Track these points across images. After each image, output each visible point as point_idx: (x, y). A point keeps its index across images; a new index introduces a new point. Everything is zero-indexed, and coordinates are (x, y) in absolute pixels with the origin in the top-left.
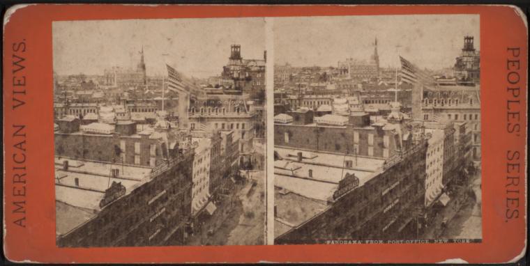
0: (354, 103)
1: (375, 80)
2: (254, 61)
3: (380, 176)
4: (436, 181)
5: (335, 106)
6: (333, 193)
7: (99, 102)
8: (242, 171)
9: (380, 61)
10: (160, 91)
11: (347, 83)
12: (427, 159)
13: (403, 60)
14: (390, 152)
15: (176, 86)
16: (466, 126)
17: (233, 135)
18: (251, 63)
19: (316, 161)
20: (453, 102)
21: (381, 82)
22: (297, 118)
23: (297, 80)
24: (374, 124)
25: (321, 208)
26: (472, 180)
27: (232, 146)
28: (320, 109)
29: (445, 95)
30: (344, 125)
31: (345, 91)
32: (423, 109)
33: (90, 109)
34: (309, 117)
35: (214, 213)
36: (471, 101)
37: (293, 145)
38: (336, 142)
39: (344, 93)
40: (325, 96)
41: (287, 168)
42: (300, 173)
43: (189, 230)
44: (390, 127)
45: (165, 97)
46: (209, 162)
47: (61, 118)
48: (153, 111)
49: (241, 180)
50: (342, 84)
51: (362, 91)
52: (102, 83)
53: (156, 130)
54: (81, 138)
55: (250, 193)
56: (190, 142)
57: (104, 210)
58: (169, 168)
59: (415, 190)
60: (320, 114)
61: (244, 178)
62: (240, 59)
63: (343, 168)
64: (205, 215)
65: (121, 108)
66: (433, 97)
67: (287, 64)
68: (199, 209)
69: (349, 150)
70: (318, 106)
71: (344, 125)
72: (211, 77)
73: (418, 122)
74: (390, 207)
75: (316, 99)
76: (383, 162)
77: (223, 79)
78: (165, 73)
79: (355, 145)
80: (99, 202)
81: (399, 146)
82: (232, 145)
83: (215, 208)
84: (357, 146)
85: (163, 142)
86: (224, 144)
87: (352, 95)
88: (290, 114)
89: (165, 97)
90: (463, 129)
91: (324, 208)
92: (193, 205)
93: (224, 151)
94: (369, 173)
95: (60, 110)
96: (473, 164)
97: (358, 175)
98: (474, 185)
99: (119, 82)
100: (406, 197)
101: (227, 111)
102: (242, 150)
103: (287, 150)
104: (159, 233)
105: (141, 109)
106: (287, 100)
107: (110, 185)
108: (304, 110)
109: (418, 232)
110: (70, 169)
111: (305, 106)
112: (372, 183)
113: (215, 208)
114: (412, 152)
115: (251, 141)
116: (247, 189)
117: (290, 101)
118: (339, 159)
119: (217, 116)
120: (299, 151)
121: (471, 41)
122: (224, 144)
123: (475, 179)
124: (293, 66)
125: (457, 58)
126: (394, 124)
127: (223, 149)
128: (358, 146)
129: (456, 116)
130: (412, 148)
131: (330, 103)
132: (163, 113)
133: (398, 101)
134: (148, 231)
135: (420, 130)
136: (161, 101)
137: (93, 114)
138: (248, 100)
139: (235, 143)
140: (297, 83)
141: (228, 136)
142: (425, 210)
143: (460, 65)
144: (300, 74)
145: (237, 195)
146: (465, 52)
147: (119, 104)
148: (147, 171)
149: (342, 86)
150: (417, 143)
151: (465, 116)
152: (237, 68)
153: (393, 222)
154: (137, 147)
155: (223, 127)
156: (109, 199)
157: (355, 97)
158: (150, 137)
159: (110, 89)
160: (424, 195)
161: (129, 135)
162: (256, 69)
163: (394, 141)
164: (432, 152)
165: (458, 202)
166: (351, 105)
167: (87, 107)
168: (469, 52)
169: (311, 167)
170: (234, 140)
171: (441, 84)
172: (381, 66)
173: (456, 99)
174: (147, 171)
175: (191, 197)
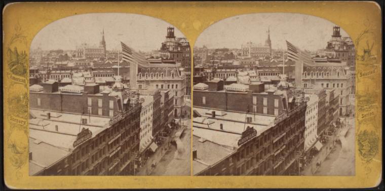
0: (253, 75)
1: (102, 59)
2: (184, 39)
3: (107, 130)
4: (312, 132)
5: (239, 77)
6: (73, 143)
7: (72, 70)
8: (176, 120)
9: (106, 47)
10: (116, 61)
11: (83, 62)
12: (306, 116)
13: (289, 44)
14: (114, 113)
15: (293, 56)
16: (334, 92)
17: (169, 93)
18: (182, 41)
19: (225, 117)
20: (160, 76)
21: (273, 60)
22: (211, 84)
23: (46, 60)
24: (267, 91)
25: (229, 152)
26: (339, 131)
27: (169, 102)
28: (63, 81)
29: (320, 69)
30: (81, 93)
31: (81, 68)
32: (138, 81)
33: (231, 73)
34: (220, 85)
35: (321, 149)
36: (338, 74)
37: (207, 105)
38: (241, 103)
39: (80, 69)
40: (67, 72)
41: (39, 124)
42: (212, 126)
43: (138, 163)
44: (279, 92)
45: (120, 65)
46: (152, 113)
47: (210, 80)
48: (111, 76)
49: (175, 126)
50: (79, 62)
51: (93, 68)
52: (240, 54)
53: (278, 88)
54: (224, 95)
55: (182, 136)
56: (138, 99)
57: (241, 148)
58: (124, 118)
59: (298, 138)
60: (64, 84)
61: (178, 125)
62: (174, 37)
63: (245, 123)
64: (151, 152)
65: (88, 74)
66: (145, 72)
67: (39, 48)
68: (310, 146)
69: (84, 112)
70: (227, 78)
71: (81, 93)
72: (153, 51)
73: (300, 89)
74: (279, 151)
75: (60, 73)
76: (110, 119)
77: (162, 52)
78: (120, 49)
79: (89, 107)
80: (237, 142)
81: (120, 108)
82: (334, 99)
83: (157, 147)
84: (255, 107)
85: (119, 98)
86: (162, 100)
87: (252, 69)
88: (207, 83)
89: (120, 65)
90: (332, 94)
91: (230, 152)
92: (306, 143)
93: (163, 105)
94: (99, 128)
95: (44, 76)
96: (175, 121)
97: (91, 129)
98: (175, 136)
99: (86, 55)
100: (127, 144)
101: (165, 76)
102: (341, 103)
103: (205, 110)
104: (116, 165)
105: (98, 74)
106: (204, 73)
107: (246, 129)
108: (217, 80)
109: (299, 169)
110: (216, 117)
111: (217, 77)
112: (266, 134)
113: (157, 147)
114: (130, 112)
115: (347, 96)
116: (179, 133)
117: (41, 75)
118: (243, 117)
119: (322, 78)
120: (48, 112)
121: (338, 30)
122: (162, 100)
123: (176, 132)
124: (208, 48)
125: (328, 42)
126: (282, 90)
127: (327, 102)
128: (91, 108)
129: (162, 86)
130: (295, 108)
131: (235, 75)
132: (284, 76)
133: (120, 75)
134: (273, 163)
135: (301, 95)
136: (117, 69)
137: (68, 78)
138: (345, 66)
139: (170, 99)
140: (212, 61)
141: (331, 92)
142: (305, 154)
143: (164, 47)
144: (214, 53)
145: (173, 137)
146: (168, 39)
147: (87, 71)
148: (107, 120)
149: (79, 64)
150: (299, 104)
151: (334, 84)
152: (172, 44)
153: (116, 163)
154: (100, 103)
155: (327, 86)
156: (80, 141)
157: (88, 72)
158: (109, 95)
159: (245, 59)
160: (139, 144)
161: (260, 92)
162: (185, 44)
163: (282, 103)
164: (144, 112)
165: (329, 148)
166: (86, 78)
167: (228, 72)
168: (336, 38)
169: (222, 122)
170: (170, 97)
171: (316, 62)
172: (107, 49)
173: (327, 72)
174: (107, 120)
175: (139, 139)
